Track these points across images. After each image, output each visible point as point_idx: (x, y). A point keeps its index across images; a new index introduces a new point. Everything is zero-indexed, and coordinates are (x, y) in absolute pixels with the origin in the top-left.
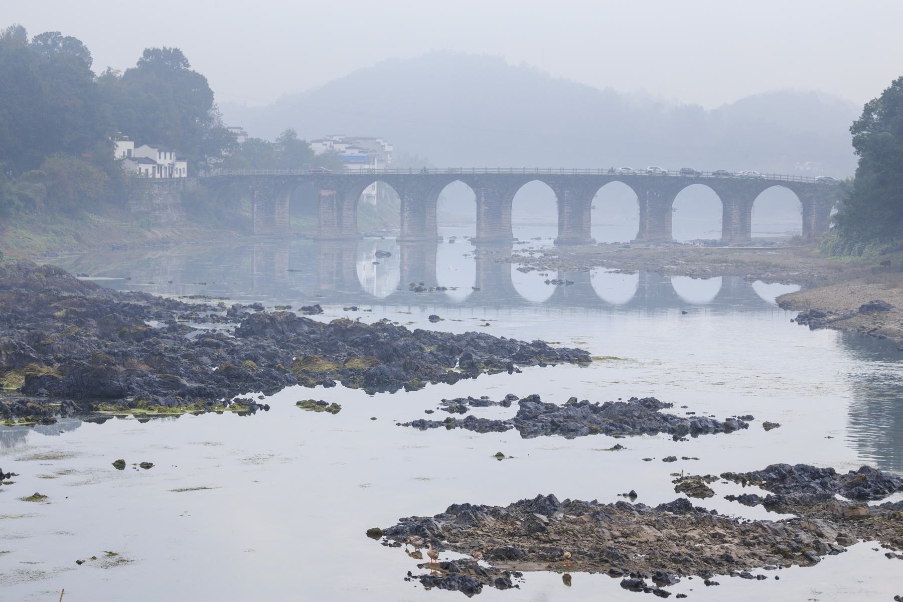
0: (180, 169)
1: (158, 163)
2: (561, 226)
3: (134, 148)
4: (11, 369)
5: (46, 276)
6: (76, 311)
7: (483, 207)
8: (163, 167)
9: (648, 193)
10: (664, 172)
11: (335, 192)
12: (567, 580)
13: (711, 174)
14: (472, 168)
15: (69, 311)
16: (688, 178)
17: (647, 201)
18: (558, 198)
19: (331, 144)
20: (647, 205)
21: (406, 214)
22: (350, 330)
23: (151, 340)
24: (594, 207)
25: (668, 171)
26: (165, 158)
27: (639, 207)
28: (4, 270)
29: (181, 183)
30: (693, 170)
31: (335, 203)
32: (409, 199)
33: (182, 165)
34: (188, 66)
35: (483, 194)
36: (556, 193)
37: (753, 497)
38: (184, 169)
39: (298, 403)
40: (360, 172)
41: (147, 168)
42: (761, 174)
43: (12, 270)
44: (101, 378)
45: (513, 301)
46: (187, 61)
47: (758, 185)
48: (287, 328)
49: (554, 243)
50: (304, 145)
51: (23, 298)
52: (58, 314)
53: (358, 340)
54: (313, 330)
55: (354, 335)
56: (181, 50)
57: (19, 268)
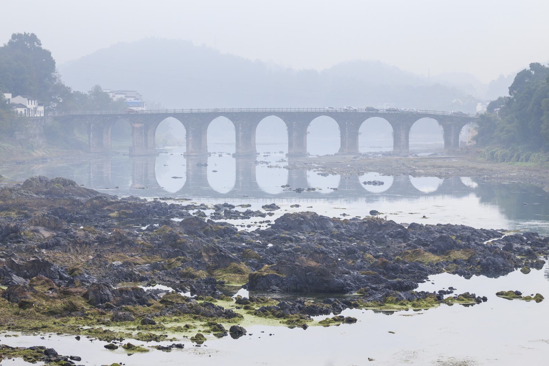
0: (40, 111)
1: (28, 107)
2: (290, 145)
3: (12, 97)
4: (218, 268)
5: (63, 185)
6: (126, 212)
7: (241, 133)
8: (30, 110)
9: (347, 123)
10: (355, 110)
12: (78, 338)
13: (385, 111)
14: (181, 109)
15: (121, 213)
16: (371, 113)
17: (347, 128)
18: (287, 127)
19: (113, 94)
20: (347, 130)
21: (190, 139)
22: (385, 226)
23: (236, 236)
24: (309, 132)
25: (358, 109)
26: (32, 104)
27: (340, 132)
28: (30, 182)
29: (43, 120)
30: (374, 108)
31: (143, 132)
32: (192, 128)
33: (41, 109)
34: (40, 45)
35: (240, 125)
36: (286, 123)
38: (42, 111)
39: (498, 294)
40: (238, 111)
41: (21, 110)
42: (417, 110)
43: (37, 182)
44: (324, 276)
46: (40, 41)
47: (414, 117)
48: (318, 224)
49: (286, 155)
50: (106, 95)
52: (112, 215)
53: (392, 233)
54: (338, 225)
55: (388, 229)
56: (35, 35)
57: (41, 181)
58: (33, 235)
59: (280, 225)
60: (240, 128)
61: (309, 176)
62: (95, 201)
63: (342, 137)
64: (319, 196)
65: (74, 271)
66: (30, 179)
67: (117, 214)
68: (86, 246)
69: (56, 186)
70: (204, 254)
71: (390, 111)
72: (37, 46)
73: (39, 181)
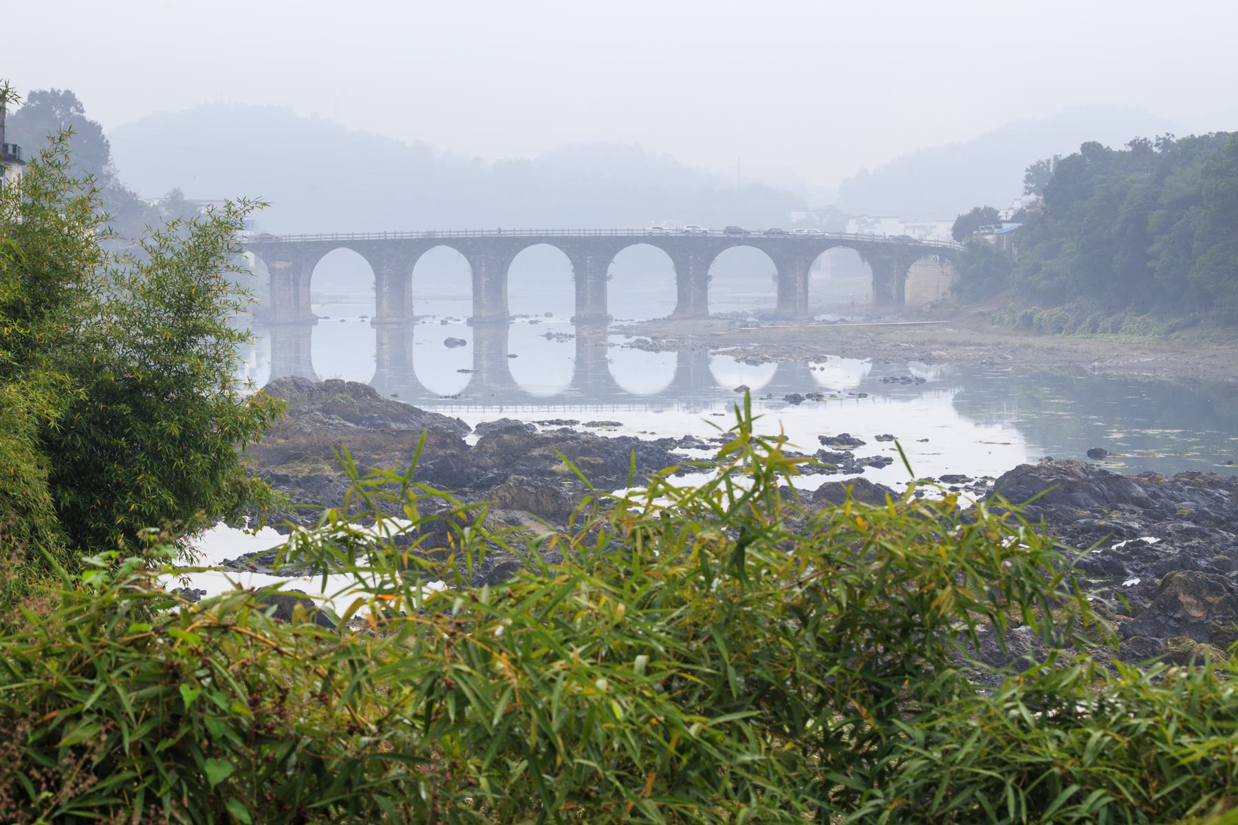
6: (589, 463)
7: (484, 279)
16: (735, 237)
21: (385, 289)
34: (82, 111)
45: (612, 394)
51: (449, 440)
58: (507, 533)
60: (483, 269)
61: (610, 361)
62: (506, 437)
64: (631, 399)
66: (274, 384)
69: (338, 397)
70: (1184, 598)
72: (77, 114)
73: (293, 388)
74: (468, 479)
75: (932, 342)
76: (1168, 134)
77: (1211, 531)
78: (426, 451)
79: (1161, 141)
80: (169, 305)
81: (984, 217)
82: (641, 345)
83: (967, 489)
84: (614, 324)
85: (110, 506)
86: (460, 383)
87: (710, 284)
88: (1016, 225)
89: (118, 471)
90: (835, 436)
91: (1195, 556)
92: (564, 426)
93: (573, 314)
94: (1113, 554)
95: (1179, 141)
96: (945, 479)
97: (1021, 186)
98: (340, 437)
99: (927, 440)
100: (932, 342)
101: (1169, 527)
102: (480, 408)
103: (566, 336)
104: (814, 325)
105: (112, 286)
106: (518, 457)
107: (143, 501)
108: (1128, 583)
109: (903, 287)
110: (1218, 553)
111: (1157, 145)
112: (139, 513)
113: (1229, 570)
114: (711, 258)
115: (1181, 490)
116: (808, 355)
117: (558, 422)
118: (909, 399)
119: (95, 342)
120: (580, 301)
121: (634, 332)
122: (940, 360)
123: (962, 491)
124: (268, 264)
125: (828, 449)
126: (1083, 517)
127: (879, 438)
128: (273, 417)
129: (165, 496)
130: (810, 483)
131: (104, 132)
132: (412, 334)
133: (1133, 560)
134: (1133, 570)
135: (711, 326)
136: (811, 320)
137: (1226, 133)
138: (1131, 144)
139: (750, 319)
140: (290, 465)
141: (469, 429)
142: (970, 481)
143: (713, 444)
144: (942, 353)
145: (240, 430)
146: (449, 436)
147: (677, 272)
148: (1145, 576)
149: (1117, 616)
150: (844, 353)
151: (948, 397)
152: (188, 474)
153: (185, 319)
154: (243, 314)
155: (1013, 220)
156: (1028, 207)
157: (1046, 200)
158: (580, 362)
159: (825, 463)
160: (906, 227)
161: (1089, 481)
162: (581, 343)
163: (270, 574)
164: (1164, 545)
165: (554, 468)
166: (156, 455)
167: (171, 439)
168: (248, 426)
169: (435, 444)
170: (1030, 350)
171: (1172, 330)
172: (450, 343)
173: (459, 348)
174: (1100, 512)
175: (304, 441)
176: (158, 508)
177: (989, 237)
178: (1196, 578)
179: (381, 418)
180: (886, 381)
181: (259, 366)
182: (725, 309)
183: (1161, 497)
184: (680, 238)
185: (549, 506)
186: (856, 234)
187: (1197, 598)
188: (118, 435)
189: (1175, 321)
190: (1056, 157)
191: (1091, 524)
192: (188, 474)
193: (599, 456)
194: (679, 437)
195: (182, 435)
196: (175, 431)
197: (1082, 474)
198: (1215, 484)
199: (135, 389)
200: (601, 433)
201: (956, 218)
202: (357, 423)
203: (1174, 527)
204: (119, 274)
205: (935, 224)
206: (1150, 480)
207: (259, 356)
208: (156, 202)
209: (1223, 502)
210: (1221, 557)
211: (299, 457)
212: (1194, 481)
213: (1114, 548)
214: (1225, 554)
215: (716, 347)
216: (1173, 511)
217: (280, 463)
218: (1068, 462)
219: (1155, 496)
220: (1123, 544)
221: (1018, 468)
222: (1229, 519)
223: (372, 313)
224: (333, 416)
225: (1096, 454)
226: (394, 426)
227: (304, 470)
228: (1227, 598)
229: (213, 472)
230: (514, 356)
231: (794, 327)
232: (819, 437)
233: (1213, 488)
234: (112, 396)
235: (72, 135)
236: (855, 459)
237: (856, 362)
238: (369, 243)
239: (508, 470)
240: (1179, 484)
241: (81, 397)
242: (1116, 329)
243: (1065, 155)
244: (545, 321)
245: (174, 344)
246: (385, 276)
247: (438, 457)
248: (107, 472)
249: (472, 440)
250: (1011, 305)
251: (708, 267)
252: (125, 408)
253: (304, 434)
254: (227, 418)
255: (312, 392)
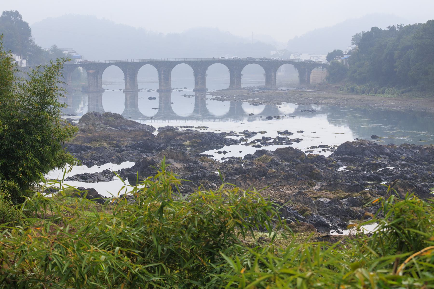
7: (163, 76)
10: (240, 59)
11: (95, 71)
16: (250, 61)
21: (128, 80)
34: (22, 18)
37: (123, 171)
51: (148, 134)
59: (343, 151)
60: (162, 72)
61: (207, 104)
62: (167, 133)
63: (231, 77)
64: (213, 118)
65: (305, 212)
67: (190, 142)
68: (256, 180)
71: (264, 59)
72: (20, 19)
73: (94, 116)
74: (154, 147)
75: (319, 97)
76: (401, 24)
77: (412, 165)
78: (139, 138)
79: (399, 26)
80: (38, 95)
81: (338, 53)
82: (217, 99)
83: (328, 150)
84: (208, 91)
85: (17, 164)
86: (154, 113)
87: (242, 77)
88: (348, 56)
89: (20, 152)
90: (283, 131)
91: (406, 174)
92: (189, 128)
93: (194, 88)
94: (377, 173)
95: (405, 27)
96: (320, 146)
97: (350, 42)
98: (109, 133)
99: (315, 133)
100: (319, 97)
101: (398, 163)
102: (161, 121)
103: (191, 96)
104: (278, 91)
105: (18, 88)
106: (171, 140)
107: (28, 163)
108: (382, 183)
109: (309, 78)
110: (414, 172)
111: (398, 28)
112: (27, 167)
113: (418, 179)
114: (242, 68)
115: (402, 150)
116: (275, 102)
117: (187, 127)
118: (311, 117)
119: (12, 108)
120: (196, 83)
121: (215, 94)
122: (322, 104)
123: (326, 151)
124: (87, 71)
125: (280, 136)
126: (368, 160)
127: (298, 132)
128: (74, 133)
129: (36, 161)
130: (272, 148)
131: (29, 25)
132: (137, 95)
133: (384, 175)
134: (384, 179)
135: (242, 92)
136: (277, 89)
137: (422, 24)
138: (388, 27)
139: (255, 89)
140: (92, 143)
141: (155, 129)
142: (329, 147)
143: (240, 134)
144: (322, 101)
145: (62, 138)
146: (148, 132)
147: (230, 73)
148: (388, 181)
149: (377, 195)
150: (288, 101)
151: (325, 116)
152: (44, 153)
153: (43, 100)
154: (63, 98)
155: (348, 54)
156: (353, 50)
157: (359, 47)
158: (196, 105)
159: (279, 141)
160: (311, 56)
161: (370, 147)
162: (196, 98)
163: (84, 182)
164: (395, 170)
165: (184, 143)
166: (33, 147)
167: (38, 141)
168: (65, 136)
169: (143, 135)
170: (353, 100)
171: (403, 93)
172: (151, 98)
173: (153, 100)
174: (374, 158)
175: (97, 134)
176: (33, 165)
177: (339, 60)
178: (404, 182)
179: (124, 126)
180: (302, 111)
181: (84, 107)
182: (247, 86)
183: (395, 153)
184: (231, 61)
185: (181, 157)
186: (293, 59)
187: (404, 189)
188: (20, 140)
189: (404, 89)
190: (363, 32)
191: (370, 162)
192: (44, 153)
193: (200, 139)
194: (228, 132)
195: (42, 140)
196: (40, 139)
197: (368, 145)
198: (415, 148)
199: (25, 125)
200: (200, 131)
201: (328, 53)
202: (116, 128)
203: (399, 163)
204: (20, 84)
205: (321, 55)
206: (392, 147)
207: (84, 104)
208: (48, 50)
209: (417, 154)
210: (415, 174)
211: (96, 140)
212: (407, 147)
213: (378, 171)
214: (416, 173)
215: (243, 100)
216: (399, 158)
217: (88, 142)
218: (363, 140)
219: (393, 152)
220: (381, 170)
221: (346, 143)
222: (419, 160)
223: (123, 88)
224: (107, 126)
225: (374, 137)
226: (129, 129)
227: (97, 145)
228: (415, 189)
229: (53, 151)
230: (173, 103)
231: (271, 92)
232: (278, 132)
233: (414, 149)
234: (18, 126)
235: (3, 37)
236: (289, 139)
237: (292, 104)
238: (122, 63)
239: (168, 144)
240: (402, 148)
241: (5, 128)
242: (383, 93)
243: (366, 31)
244: (184, 90)
245: (39, 108)
246: (128, 75)
247: (144, 140)
248: (16, 152)
249: (156, 133)
250: (347, 84)
251: (241, 71)
252: (22, 131)
253: (97, 132)
254: (57, 134)
255: (100, 117)
